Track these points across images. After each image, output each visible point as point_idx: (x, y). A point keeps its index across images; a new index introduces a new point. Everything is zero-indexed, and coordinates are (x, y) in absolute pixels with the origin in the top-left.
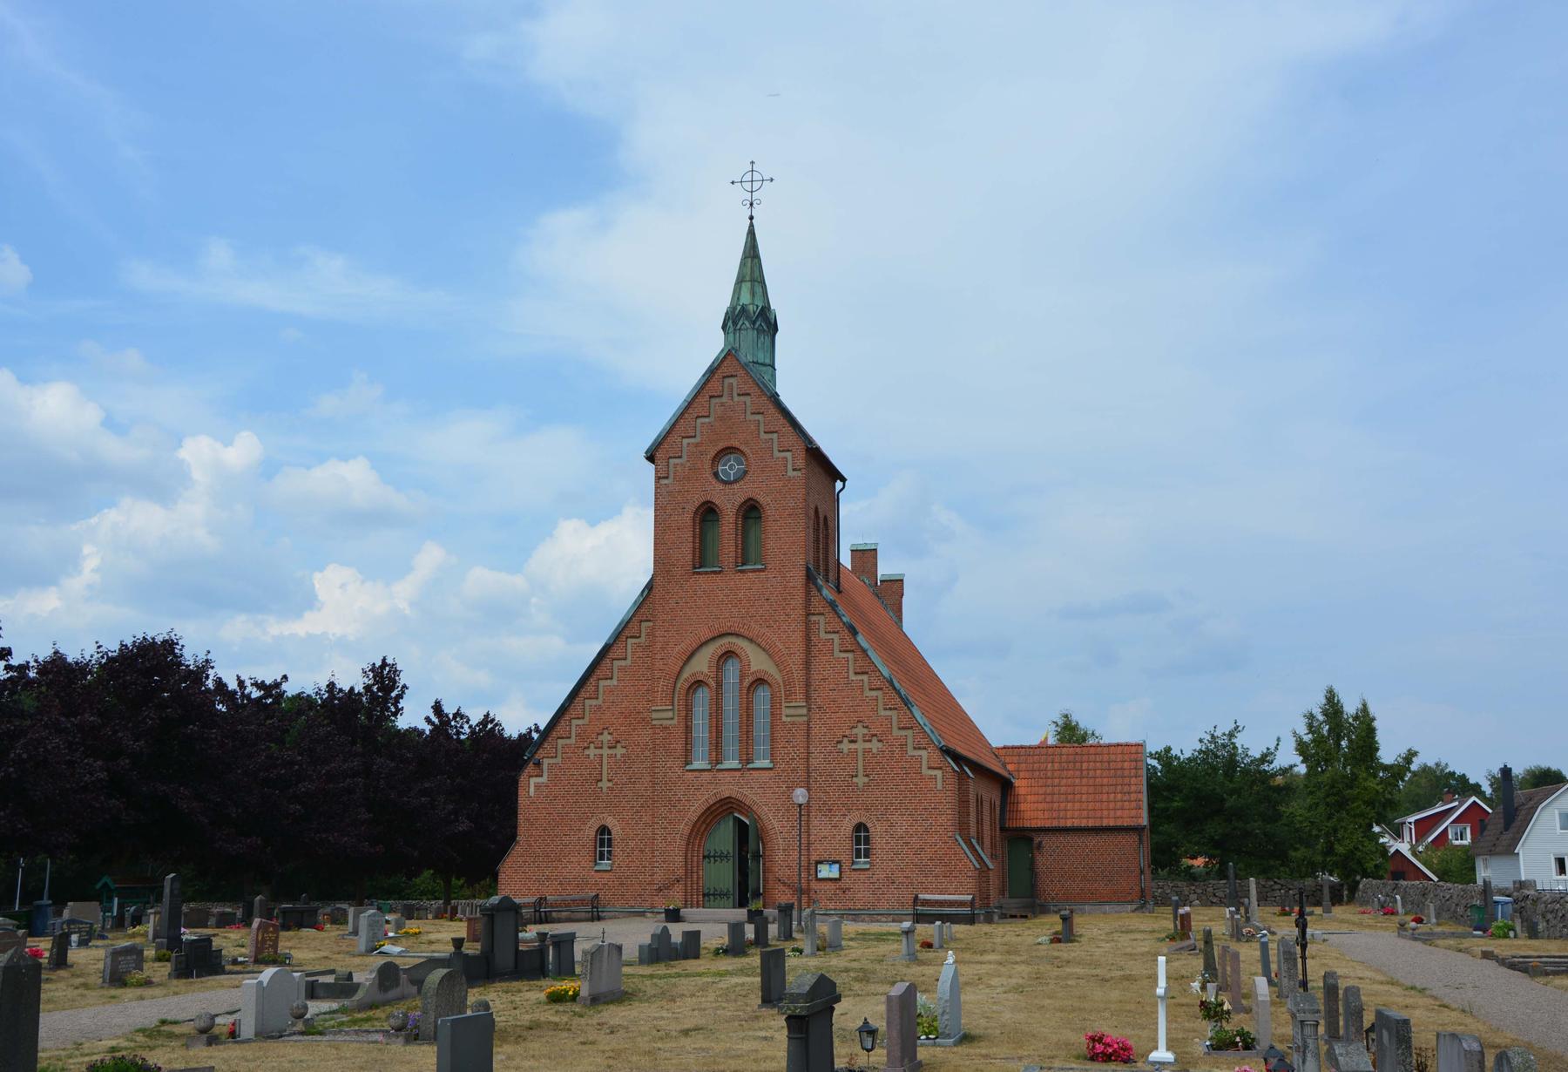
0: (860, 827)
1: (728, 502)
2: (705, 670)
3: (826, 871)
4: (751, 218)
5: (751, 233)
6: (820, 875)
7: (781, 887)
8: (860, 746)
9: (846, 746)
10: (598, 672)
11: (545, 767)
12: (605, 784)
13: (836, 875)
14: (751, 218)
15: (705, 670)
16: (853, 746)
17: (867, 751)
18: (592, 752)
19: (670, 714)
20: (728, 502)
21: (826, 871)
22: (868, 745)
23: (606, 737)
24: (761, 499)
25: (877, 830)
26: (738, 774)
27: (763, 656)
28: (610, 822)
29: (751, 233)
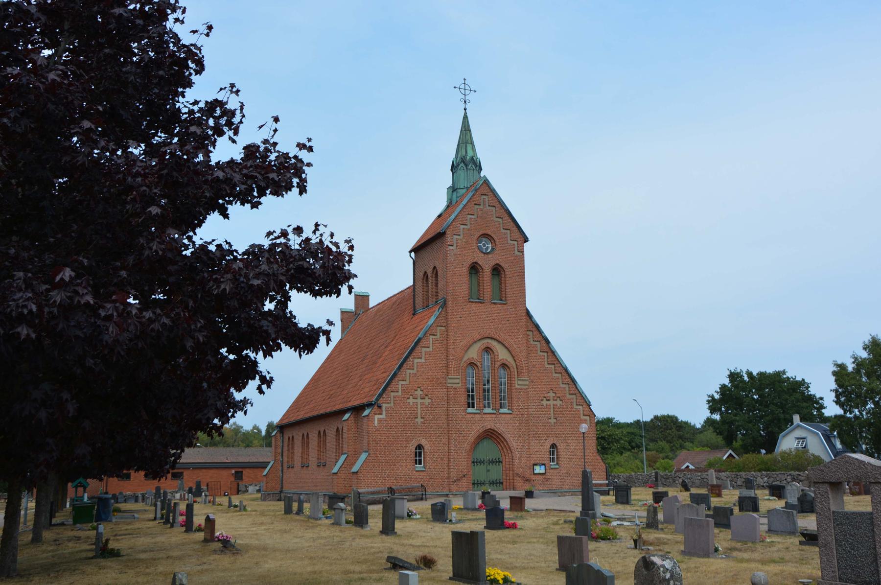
0: (553, 446)
1: (487, 265)
2: (476, 357)
3: (539, 470)
4: (465, 109)
5: (465, 117)
6: (536, 472)
7: (518, 479)
8: (551, 402)
9: (545, 402)
10: (414, 354)
11: (384, 408)
12: (419, 420)
13: (543, 471)
14: (465, 109)
15: (476, 357)
16: (548, 402)
17: (554, 406)
18: (411, 401)
19: (457, 381)
20: (487, 265)
21: (539, 470)
22: (555, 402)
23: (419, 392)
24: (502, 264)
25: (561, 446)
26: (494, 416)
27: (505, 351)
28: (424, 442)
29: (465, 117)
